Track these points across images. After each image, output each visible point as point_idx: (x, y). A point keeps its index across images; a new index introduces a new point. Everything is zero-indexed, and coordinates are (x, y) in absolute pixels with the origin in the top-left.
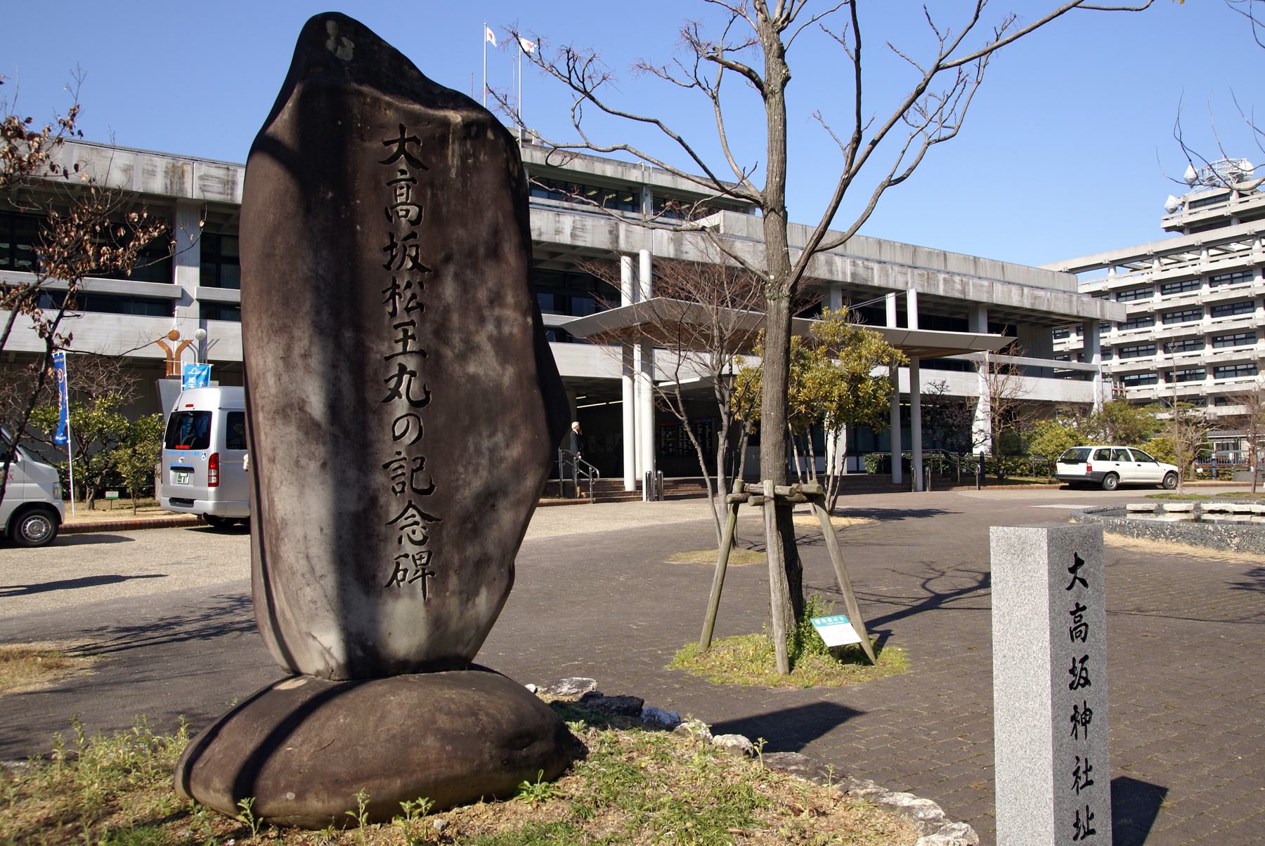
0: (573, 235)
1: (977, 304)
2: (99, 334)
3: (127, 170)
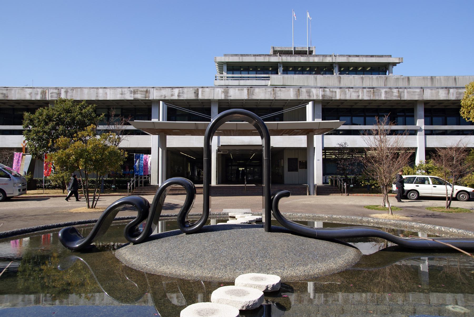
0: (178, 96)
1: (414, 103)
2: (393, 141)
3: (30, 94)
